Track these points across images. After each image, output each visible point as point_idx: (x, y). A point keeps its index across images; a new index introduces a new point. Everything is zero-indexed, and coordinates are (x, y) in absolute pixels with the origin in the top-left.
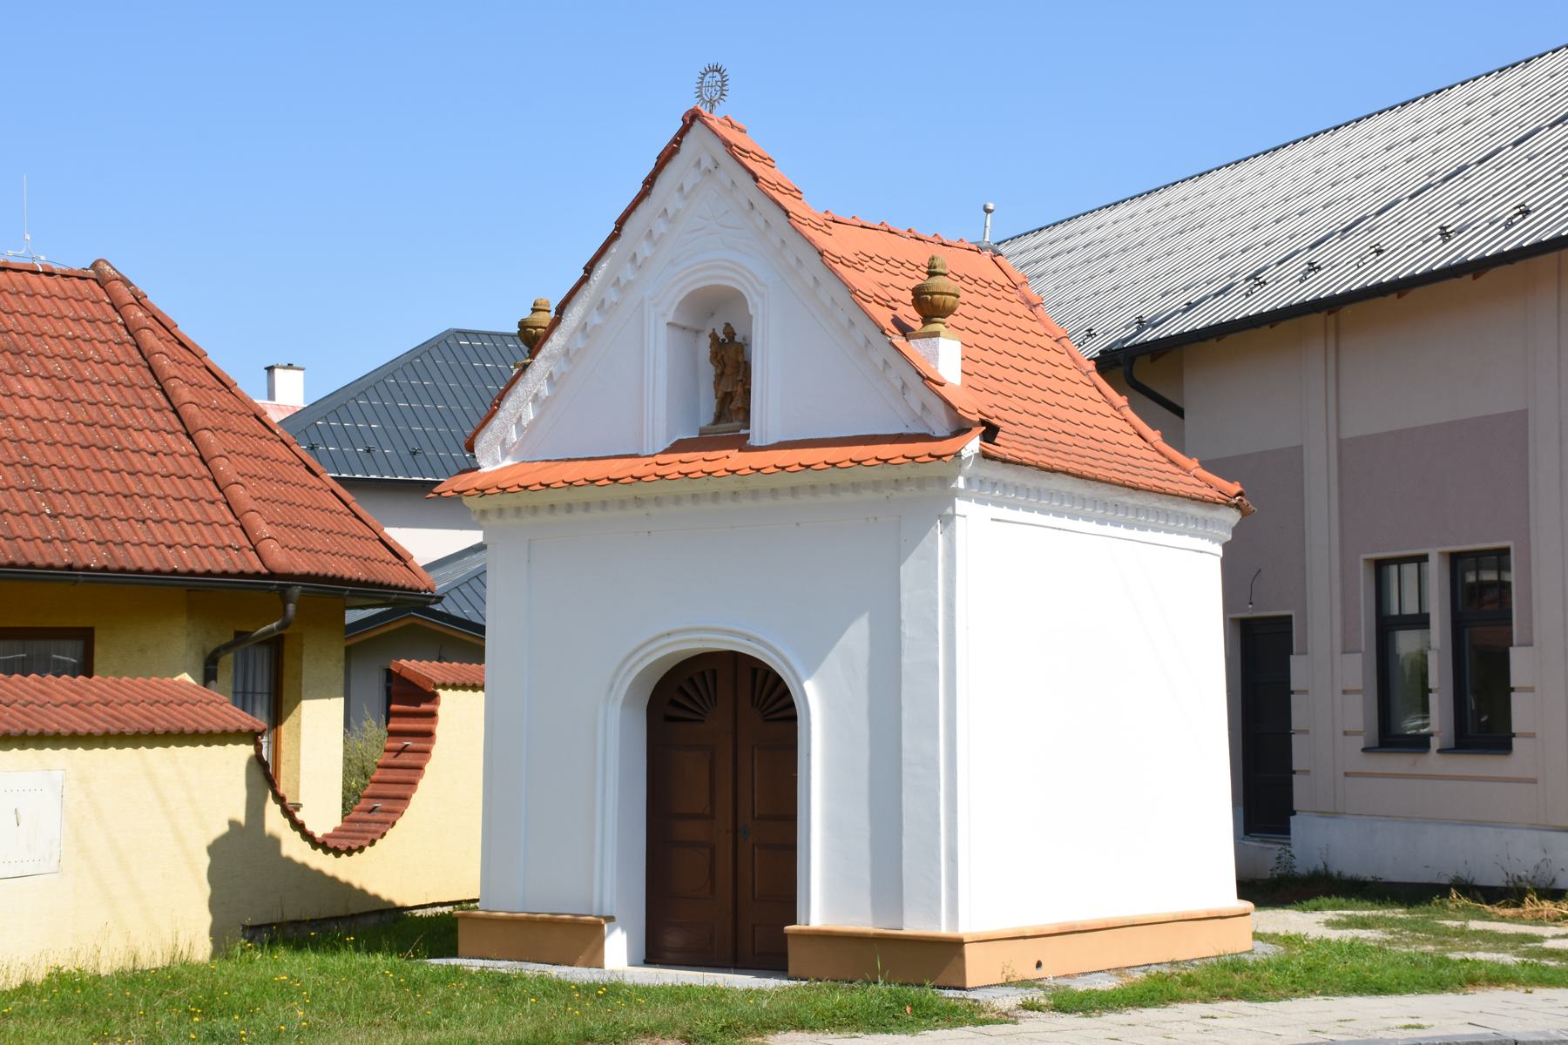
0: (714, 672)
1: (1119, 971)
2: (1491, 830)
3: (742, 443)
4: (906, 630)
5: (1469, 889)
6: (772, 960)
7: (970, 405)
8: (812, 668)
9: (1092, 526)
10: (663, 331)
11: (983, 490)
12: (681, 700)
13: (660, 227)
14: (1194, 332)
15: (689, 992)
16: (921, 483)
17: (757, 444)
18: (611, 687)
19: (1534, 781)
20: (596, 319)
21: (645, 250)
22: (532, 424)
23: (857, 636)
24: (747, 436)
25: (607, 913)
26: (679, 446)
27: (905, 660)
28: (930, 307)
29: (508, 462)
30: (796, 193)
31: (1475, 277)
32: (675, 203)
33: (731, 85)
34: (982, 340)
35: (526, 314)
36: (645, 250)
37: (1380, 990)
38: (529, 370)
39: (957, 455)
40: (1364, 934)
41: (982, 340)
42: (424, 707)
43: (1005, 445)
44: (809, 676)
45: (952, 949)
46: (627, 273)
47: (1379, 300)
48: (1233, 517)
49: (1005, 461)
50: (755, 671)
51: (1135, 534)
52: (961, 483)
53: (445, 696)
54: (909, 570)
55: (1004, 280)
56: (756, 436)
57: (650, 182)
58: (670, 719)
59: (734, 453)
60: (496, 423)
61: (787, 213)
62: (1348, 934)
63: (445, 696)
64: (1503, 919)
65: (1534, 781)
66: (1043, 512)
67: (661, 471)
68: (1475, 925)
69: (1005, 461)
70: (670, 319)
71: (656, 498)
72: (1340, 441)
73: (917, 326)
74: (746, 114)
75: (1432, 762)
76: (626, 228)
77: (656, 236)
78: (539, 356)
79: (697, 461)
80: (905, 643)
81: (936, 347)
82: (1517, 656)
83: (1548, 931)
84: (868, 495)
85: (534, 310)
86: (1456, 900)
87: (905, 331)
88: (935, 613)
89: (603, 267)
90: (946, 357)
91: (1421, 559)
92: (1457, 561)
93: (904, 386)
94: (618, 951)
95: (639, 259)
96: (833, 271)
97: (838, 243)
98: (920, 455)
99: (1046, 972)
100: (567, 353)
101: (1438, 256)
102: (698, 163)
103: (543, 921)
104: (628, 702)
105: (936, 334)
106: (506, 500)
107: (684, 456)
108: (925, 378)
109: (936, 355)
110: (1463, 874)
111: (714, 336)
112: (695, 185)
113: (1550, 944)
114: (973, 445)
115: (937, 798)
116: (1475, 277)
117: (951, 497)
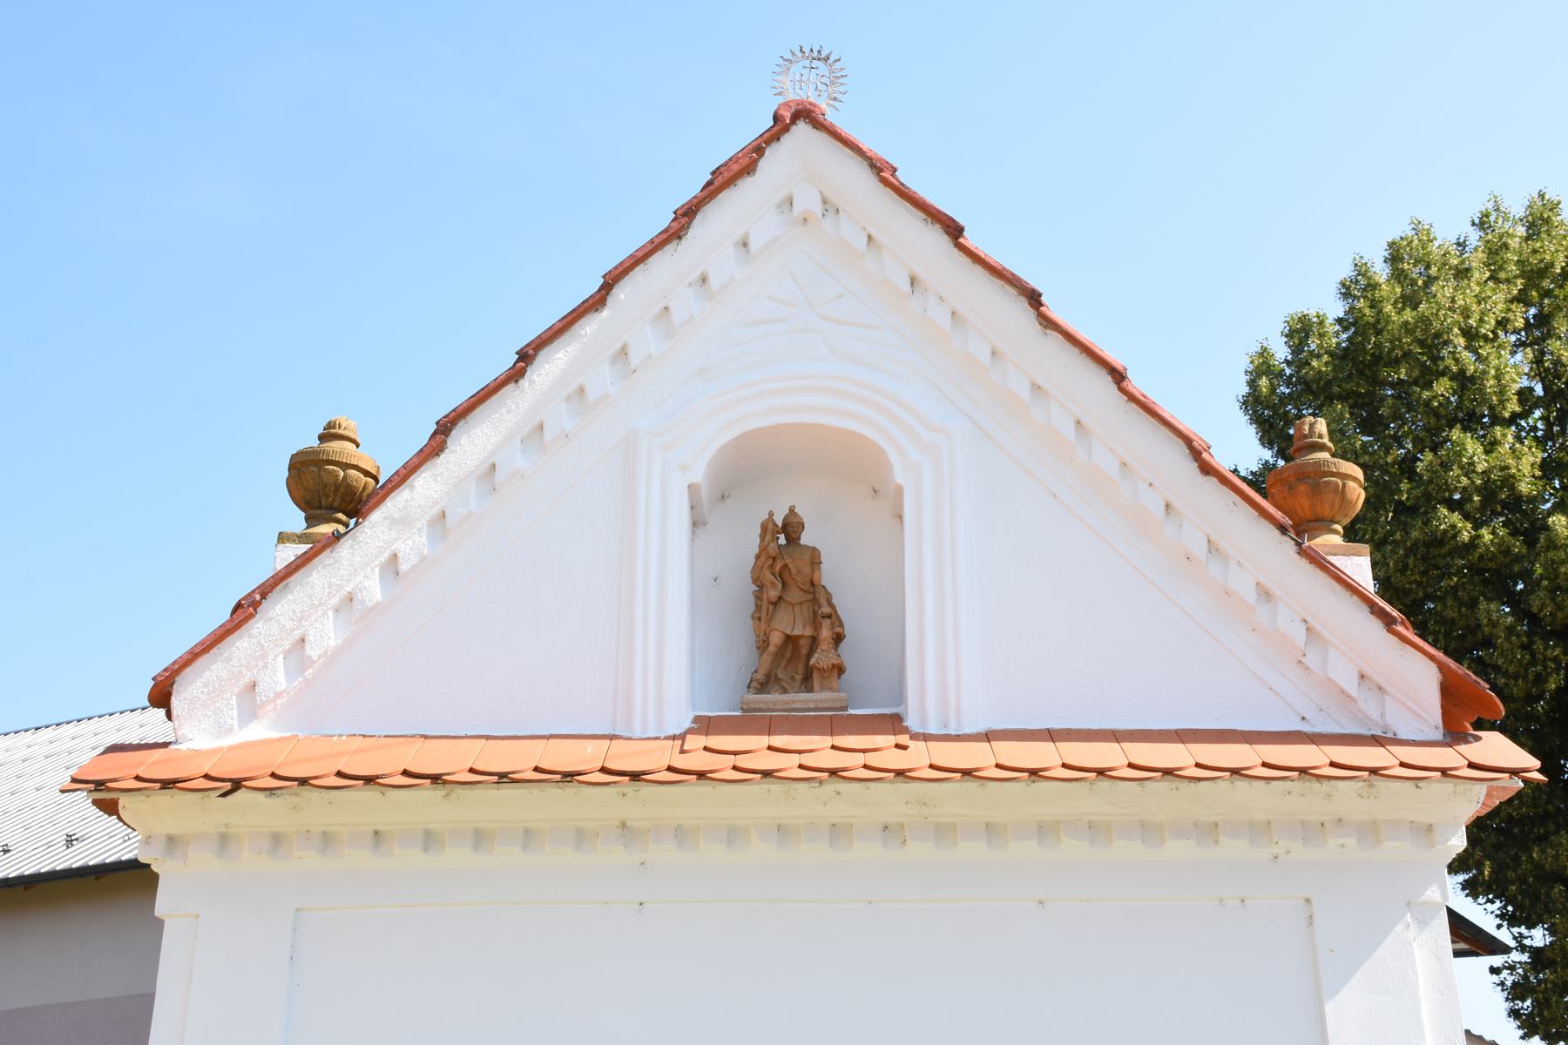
26: (705, 725)
57: (688, 214)
76: (621, 293)
85: (323, 438)
102: (790, 202)
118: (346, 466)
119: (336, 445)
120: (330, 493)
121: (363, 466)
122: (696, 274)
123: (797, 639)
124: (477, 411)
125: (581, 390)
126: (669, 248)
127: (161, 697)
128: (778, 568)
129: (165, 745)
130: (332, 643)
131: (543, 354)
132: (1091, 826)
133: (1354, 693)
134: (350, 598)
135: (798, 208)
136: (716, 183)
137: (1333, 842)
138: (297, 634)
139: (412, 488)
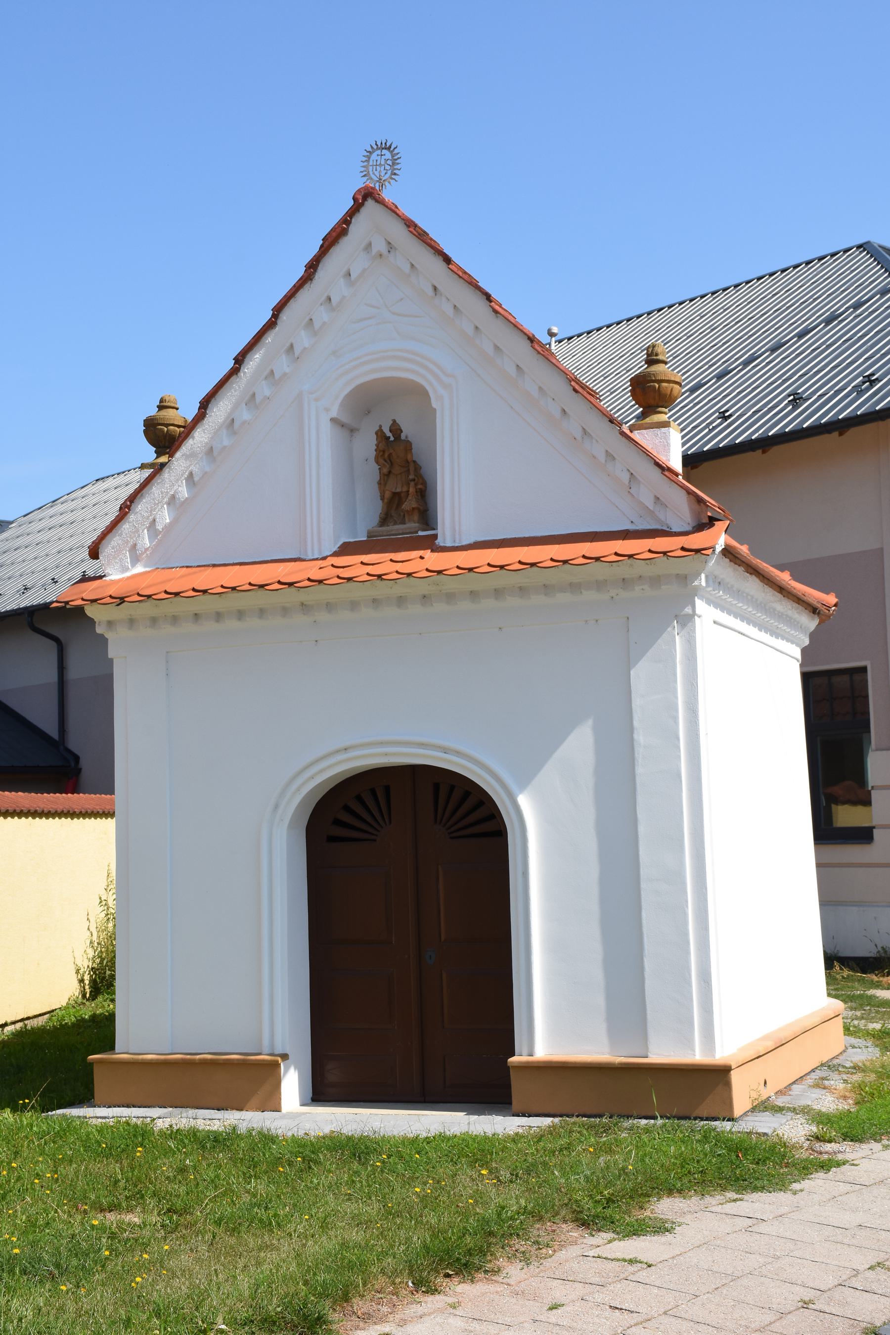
0: (387, 789)
2: (855, 909)
3: (430, 543)
4: (640, 737)
8: (525, 781)
10: (326, 428)
12: (345, 817)
13: (322, 316)
16: (656, 581)
17: (449, 544)
18: (276, 807)
20: (245, 415)
21: (303, 340)
22: (168, 528)
23: (580, 745)
24: (435, 537)
25: (279, 1050)
26: (346, 549)
27: (639, 770)
29: (139, 569)
31: (841, 434)
33: (403, 163)
35: (153, 411)
36: (303, 340)
38: (166, 470)
44: (522, 789)
45: (717, 1077)
46: (282, 365)
47: (750, 454)
54: (641, 674)
56: (445, 534)
57: (313, 267)
58: (332, 839)
59: (427, 554)
70: (334, 413)
71: (328, 604)
76: (284, 316)
77: (317, 324)
78: (178, 455)
80: (640, 752)
84: (590, 595)
85: (161, 408)
88: (675, 719)
89: (255, 359)
100: (210, 451)
101: (859, 406)
102: (369, 245)
103: (204, 1062)
104: (291, 826)
105: (666, 425)
106: (148, 609)
111: (380, 434)
112: (364, 270)
115: (685, 914)
116: (841, 434)
118: (167, 425)
119: (164, 413)
120: (164, 438)
121: (176, 423)
122: (324, 298)
123: (402, 491)
124: (220, 392)
125: (272, 372)
126: (307, 286)
127: (94, 553)
128: (386, 455)
129: (101, 577)
130: (168, 521)
131: (248, 356)
132: (521, 588)
133: (651, 508)
134: (173, 497)
135: (374, 251)
136: (325, 246)
137: (637, 588)
138: (151, 518)
139: (193, 438)
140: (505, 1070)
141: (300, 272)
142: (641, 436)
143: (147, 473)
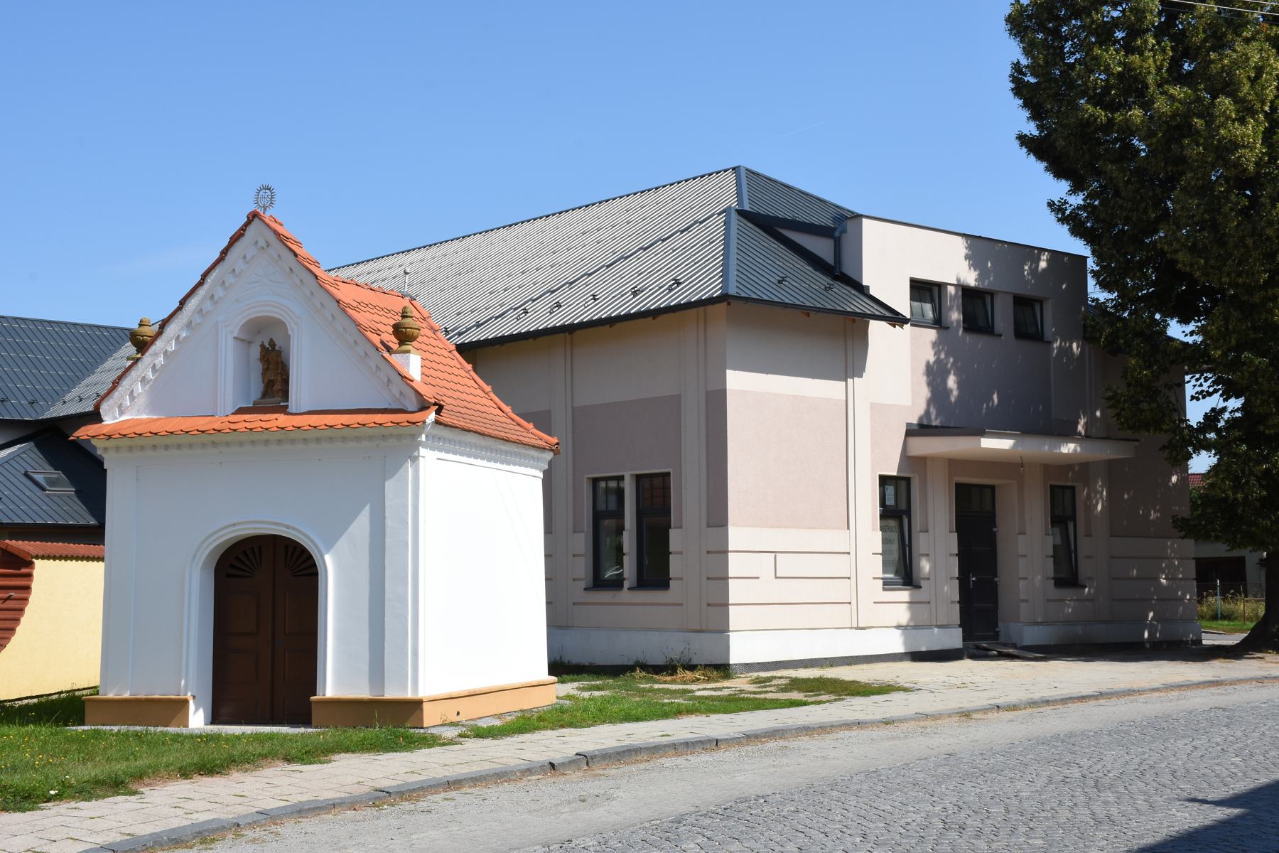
0: (260, 548)
1: (500, 716)
3: (284, 410)
4: (388, 522)
5: (644, 667)
6: (302, 716)
7: (429, 393)
9: (484, 463)
10: (231, 342)
11: (435, 443)
13: (230, 280)
14: (486, 340)
15: (271, 737)
16: (399, 437)
18: (195, 556)
19: (681, 605)
23: (361, 525)
27: (387, 540)
28: (403, 335)
30: (316, 264)
32: (240, 266)
34: (431, 357)
37: (638, 719)
39: (424, 422)
40: (597, 693)
41: (431, 357)
42: (24, 571)
43: (445, 417)
44: (328, 551)
46: (208, 306)
48: (549, 456)
49: (446, 425)
50: (287, 547)
51: (505, 467)
52: (423, 438)
53: (38, 564)
55: (418, 315)
57: (224, 253)
58: (229, 576)
60: (116, 394)
61: (316, 277)
62: (586, 695)
63: (38, 564)
64: (665, 682)
65: (681, 605)
66: (462, 455)
67: (233, 426)
68: (656, 686)
69: (446, 425)
72: (573, 408)
73: (395, 347)
74: (284, 215)
75: (625, 595)
79: (256, 420)
81: (408, 359)
82: (673, 533)
83: (694, 687)
85: (140, 325)
86: (639, 673)
87: (389, 349)
88: (407, 513)
90: (413, 365)
91: (621, 478)
92: (639, 478)
93: (389, 380)
94: (197, 720)
95: (216, 298)
96: (344, 311)
97: (345, 294)
98: (398, 423)
99: (462, 718)
101: (634, 306)
102: (256, 243)
104: (203, 568)
105: (408, 352)
106: (125, 442)
107: (247, 417)
108: (403, 377)
109: (408, 364)
110: (641, 660)
111: (262, 346)
113: (698, 694)
114: (431, 417)
117: (417, 446)
140: (309, 704)
141: (217, 255)
142: (395, 359)
143: (129, 363)
